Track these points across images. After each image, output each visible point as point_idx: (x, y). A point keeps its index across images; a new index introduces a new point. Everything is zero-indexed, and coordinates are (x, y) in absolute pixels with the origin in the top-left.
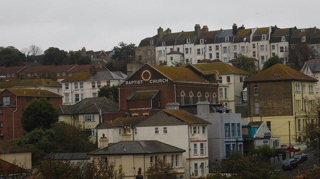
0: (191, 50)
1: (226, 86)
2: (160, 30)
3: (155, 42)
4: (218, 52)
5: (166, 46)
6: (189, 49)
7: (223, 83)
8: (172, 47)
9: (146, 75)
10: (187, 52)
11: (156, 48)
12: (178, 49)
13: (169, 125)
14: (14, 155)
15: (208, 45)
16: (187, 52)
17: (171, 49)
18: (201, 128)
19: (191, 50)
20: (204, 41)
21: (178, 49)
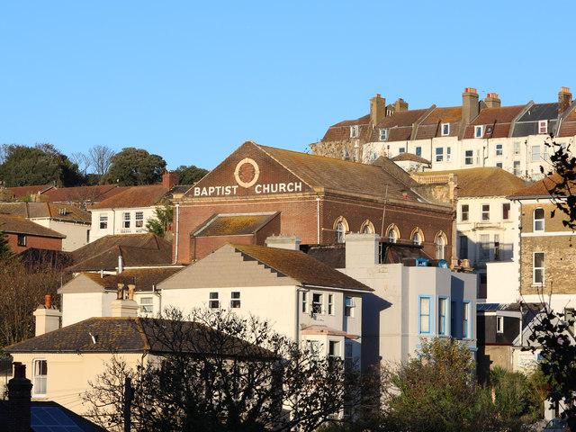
0: (449, 152)
1: (498, 228)
2: (379, 101)
3: (364, 131)
4: (517, 159)
5: (389, 140)
6: (445, 151)
7: (490, 221)
8: (402, 144)
9: (247, 173)
10: (439, 159)
11: (365, 146)
12: (419, 150)
13: (245, 285)
14: (501, 347)
15: (495, 142)
16: (439, 159)
17: (402, 150)
18: (338, 298)
19: (449, 152)
20: (486, 132)
21: (419, 150)
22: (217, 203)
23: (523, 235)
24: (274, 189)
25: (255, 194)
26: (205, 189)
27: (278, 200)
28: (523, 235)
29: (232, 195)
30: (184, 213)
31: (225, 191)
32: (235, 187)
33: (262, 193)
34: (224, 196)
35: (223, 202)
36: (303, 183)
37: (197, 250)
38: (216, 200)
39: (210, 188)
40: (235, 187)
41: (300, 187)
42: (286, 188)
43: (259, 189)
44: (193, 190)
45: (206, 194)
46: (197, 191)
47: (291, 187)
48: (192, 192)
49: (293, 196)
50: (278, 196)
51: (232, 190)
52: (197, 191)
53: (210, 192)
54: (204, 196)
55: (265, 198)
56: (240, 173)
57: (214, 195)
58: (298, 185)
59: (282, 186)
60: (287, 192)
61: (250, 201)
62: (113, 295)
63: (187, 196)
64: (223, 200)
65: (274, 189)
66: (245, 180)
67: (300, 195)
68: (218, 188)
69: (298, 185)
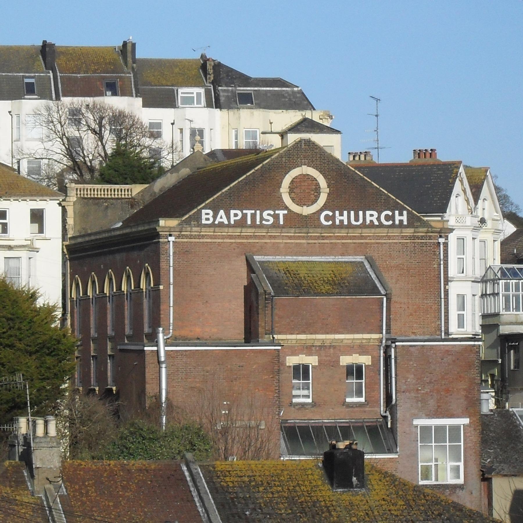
22: (247, 237)
23: (155, 348)
24: (357, 219)
25: (320, 226)
26: (222, 213)
27: (365, 238)
28: (155, 348)
29: (275, 225)
30: (182, 251)
31: (262, 219)
32: (281, 213)
33: (334, 226)
34: (261, 226)
35: (259, 237)
36: (409, 213)
37: (276, 318)
38: (249, 232)
39: (232, 212)
40: (281, 213)
41: (405, 218)
42: (378, 219)
43: (327, 218)
44: (199, 212)
45: (226, 222)
46: (207, 215)
47: (387, 218)
48: (198, 217)
49: (395, 232)
50: (366, 232)
51: (276, 217)
52: (207, 215)
53: (233, 219)
54: (221, 225)
55: (343, 233)
56: (291, 190)
57: (241, 223)
58: (401, 214)
59: (371, 216)
60: (381, 226)
61: (312, 238)
62: (414, 485)
63: (188, 222)
64: (262, 232)
65: (357, 219)
66: (300, 202)
67: (409, 232)
68: (249, 212)
69: (401, 214)
